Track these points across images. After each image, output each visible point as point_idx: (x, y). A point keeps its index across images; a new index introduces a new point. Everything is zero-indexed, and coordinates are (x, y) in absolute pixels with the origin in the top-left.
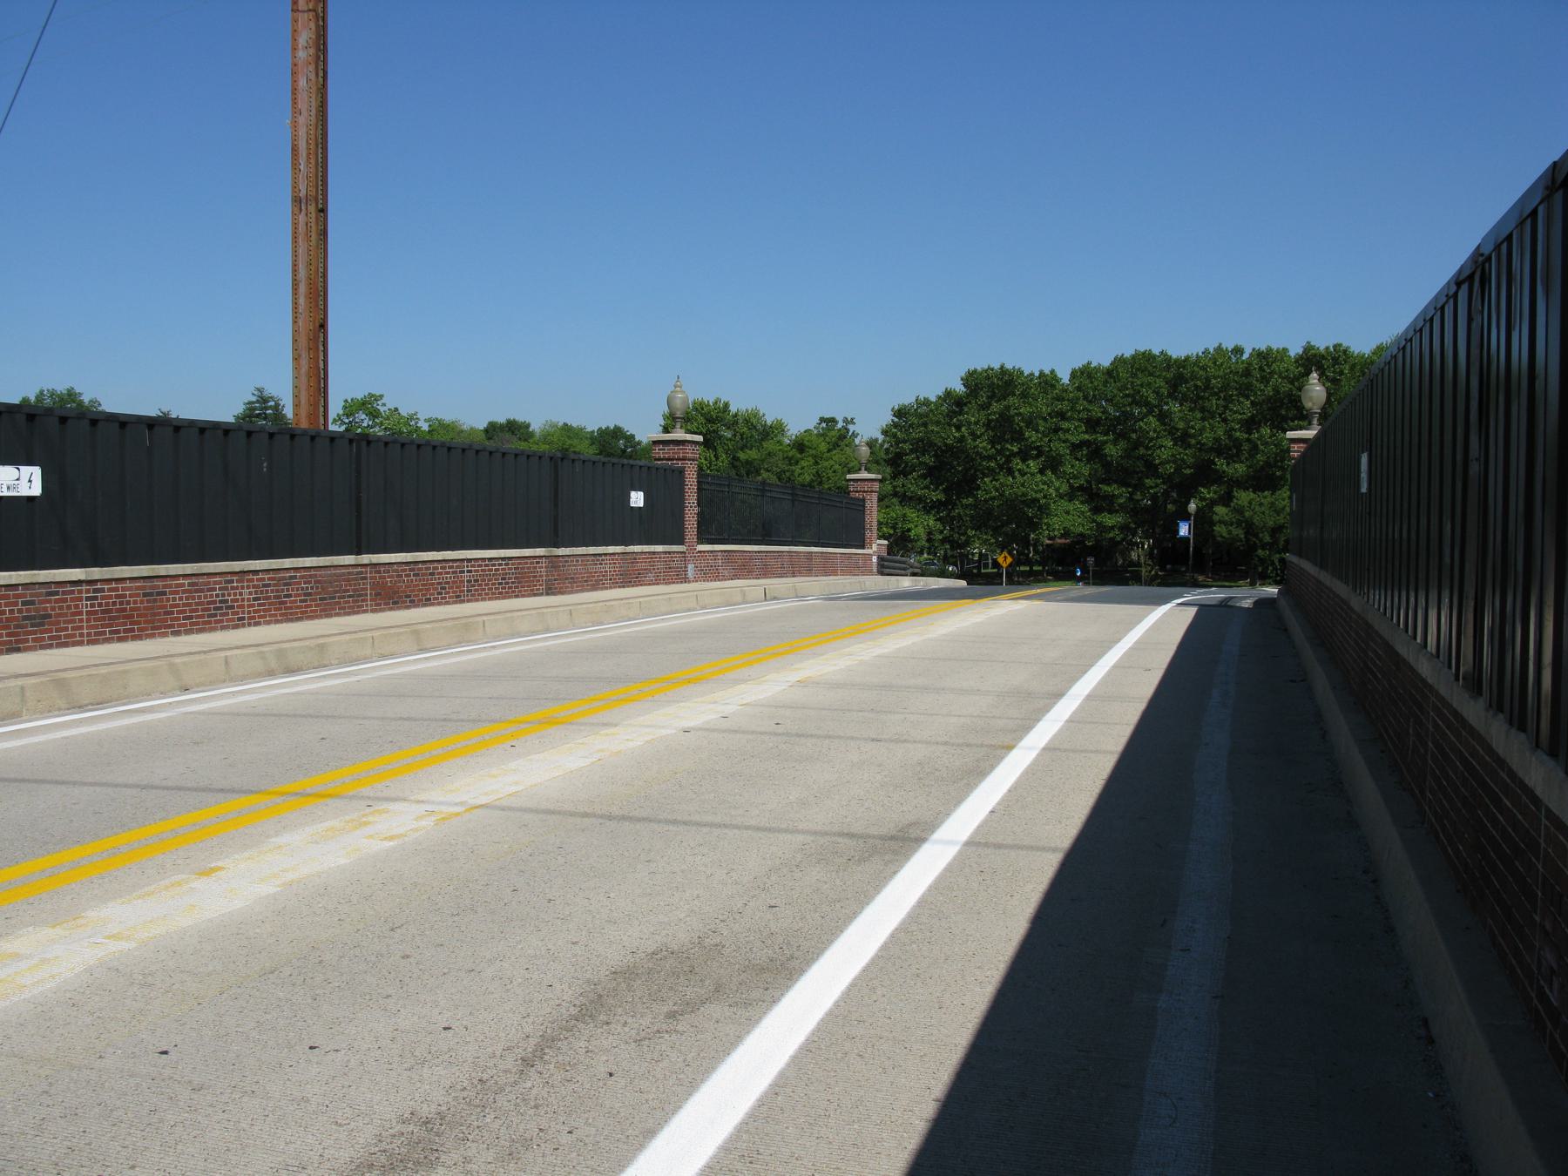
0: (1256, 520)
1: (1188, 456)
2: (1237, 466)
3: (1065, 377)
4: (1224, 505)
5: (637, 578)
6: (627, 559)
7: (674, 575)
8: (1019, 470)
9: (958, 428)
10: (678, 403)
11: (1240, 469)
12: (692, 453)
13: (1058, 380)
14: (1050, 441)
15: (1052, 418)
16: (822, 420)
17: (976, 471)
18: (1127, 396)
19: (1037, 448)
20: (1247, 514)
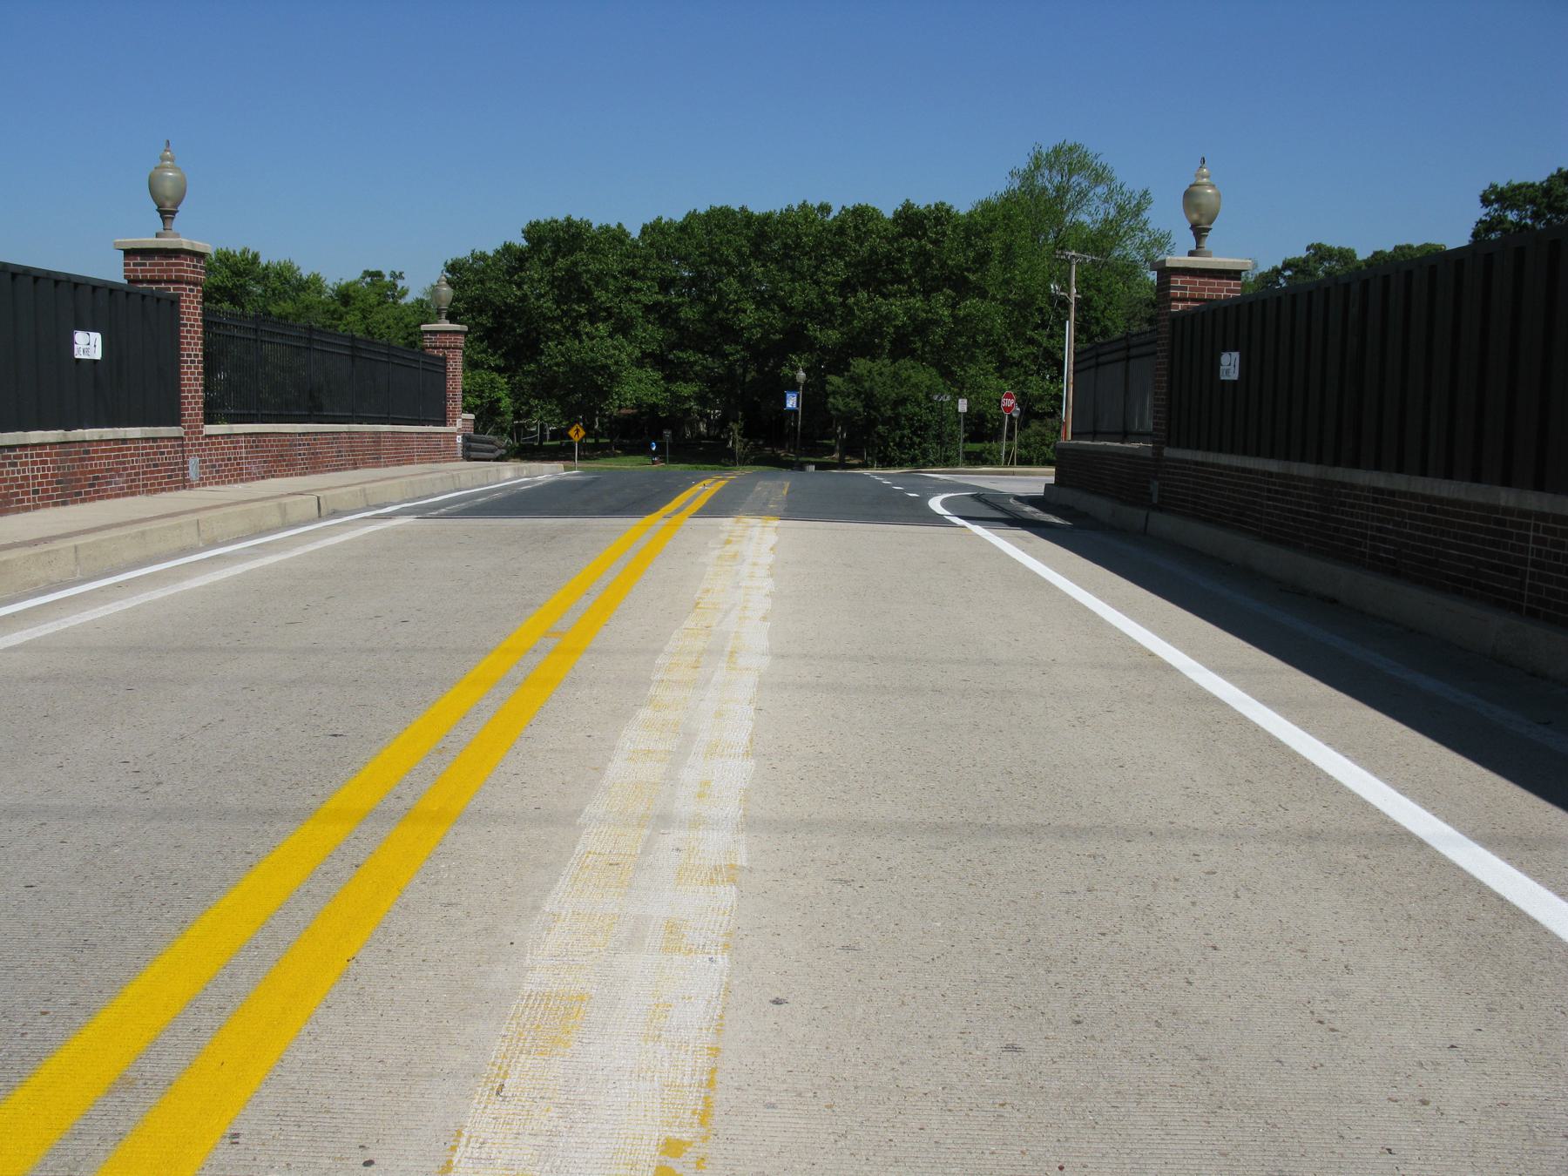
1: (776, 318)
3: (635, 233)
5: (92, 485)
6: (69, 454)
7: (163, 477)
8: (587, 333)
9: (519, 286)
12: (193, 272)
13: (627, 235)
16: (367, 273)
17: (539, 334)
19: (607, 310)
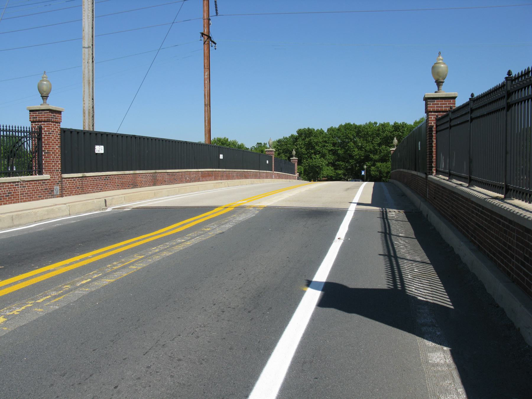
0: (382, 170)
1: (362, 153)
2: (376, 156)
3: (326, 131)
4: (374, 167)
8: (314, 158)
9: (296, 146)
10: (270, 143)
11: (377, 157)
14: (322, 149)
15: (323, 143)
16: (258, 143)
18: (344, 136)
19: (319, 151)
20: (380, 169)
